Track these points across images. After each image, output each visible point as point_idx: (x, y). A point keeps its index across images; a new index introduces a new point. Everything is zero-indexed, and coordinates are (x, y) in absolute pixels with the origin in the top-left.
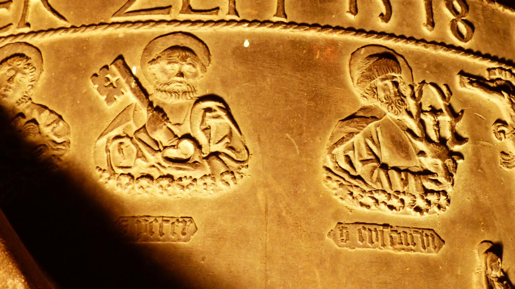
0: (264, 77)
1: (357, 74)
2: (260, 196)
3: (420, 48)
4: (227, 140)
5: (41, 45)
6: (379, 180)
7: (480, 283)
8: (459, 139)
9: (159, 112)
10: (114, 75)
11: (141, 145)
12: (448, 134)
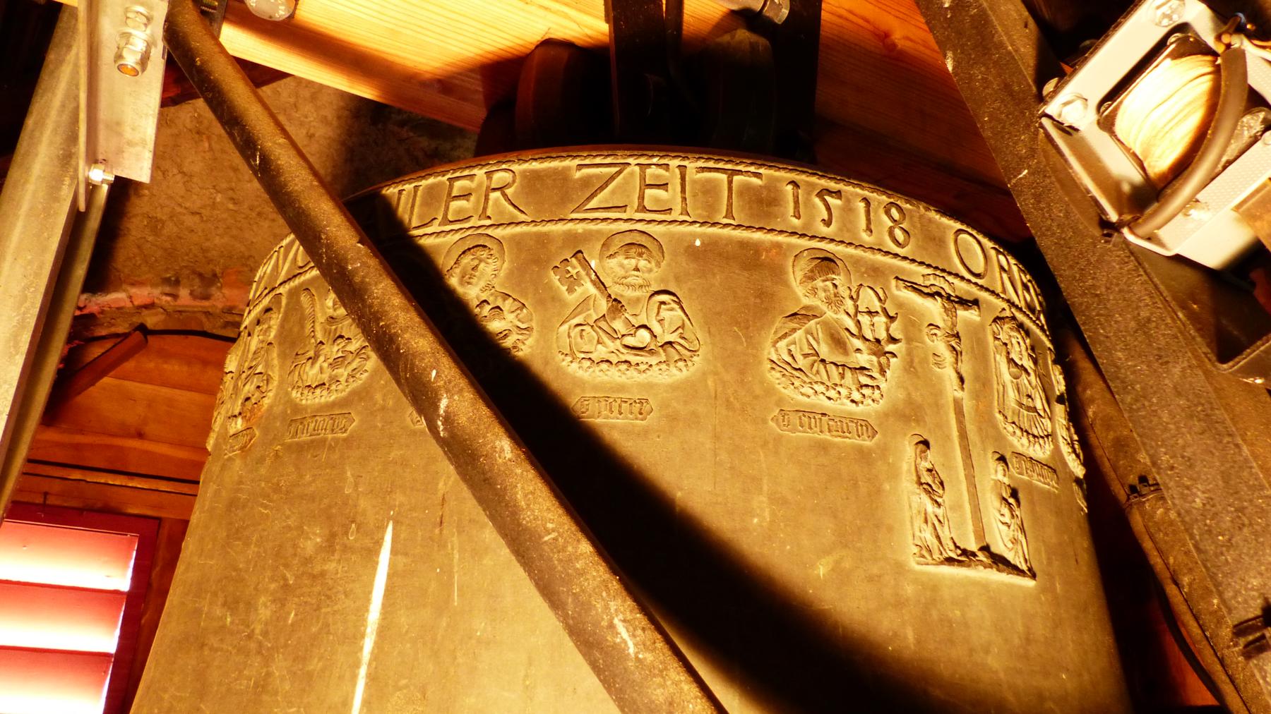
0: (714, 275)
1: (799, 275)
2: (710, 383)
3: (859, 252)
4: (680, 331)
5: (503, 237)
6: (818, 372)
7: (909, 471)
8: (893, 340)
9: (617, 305)
10: (574, 268)
11: (601, 332)
12: (883, 335)
